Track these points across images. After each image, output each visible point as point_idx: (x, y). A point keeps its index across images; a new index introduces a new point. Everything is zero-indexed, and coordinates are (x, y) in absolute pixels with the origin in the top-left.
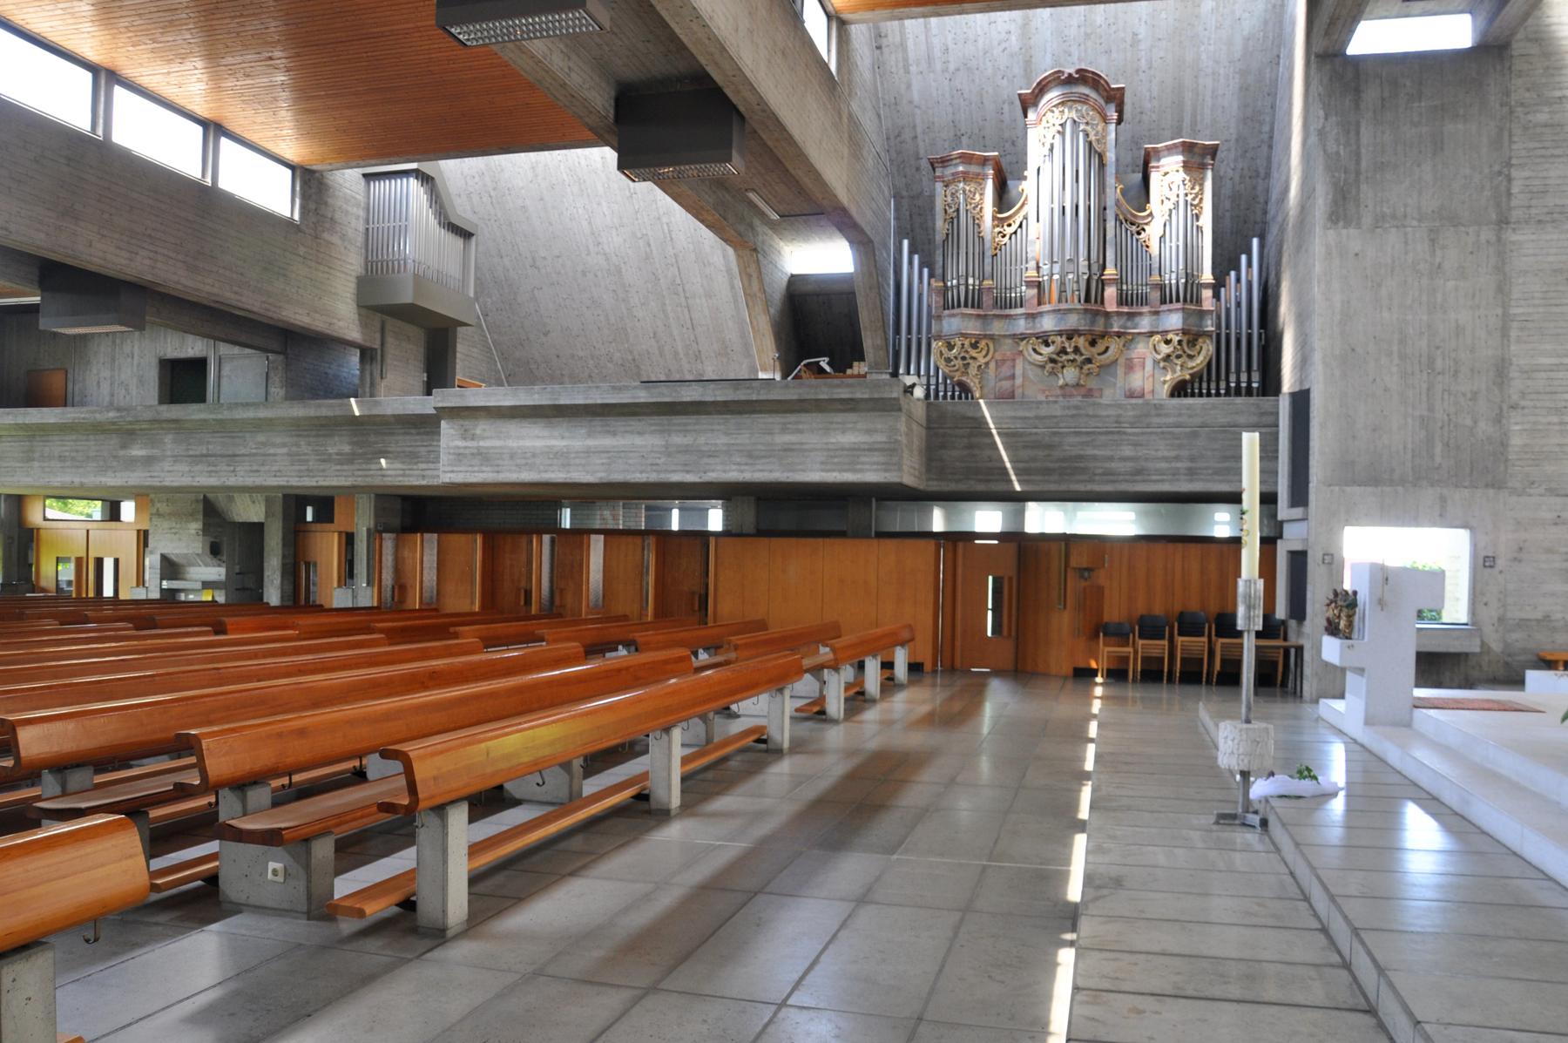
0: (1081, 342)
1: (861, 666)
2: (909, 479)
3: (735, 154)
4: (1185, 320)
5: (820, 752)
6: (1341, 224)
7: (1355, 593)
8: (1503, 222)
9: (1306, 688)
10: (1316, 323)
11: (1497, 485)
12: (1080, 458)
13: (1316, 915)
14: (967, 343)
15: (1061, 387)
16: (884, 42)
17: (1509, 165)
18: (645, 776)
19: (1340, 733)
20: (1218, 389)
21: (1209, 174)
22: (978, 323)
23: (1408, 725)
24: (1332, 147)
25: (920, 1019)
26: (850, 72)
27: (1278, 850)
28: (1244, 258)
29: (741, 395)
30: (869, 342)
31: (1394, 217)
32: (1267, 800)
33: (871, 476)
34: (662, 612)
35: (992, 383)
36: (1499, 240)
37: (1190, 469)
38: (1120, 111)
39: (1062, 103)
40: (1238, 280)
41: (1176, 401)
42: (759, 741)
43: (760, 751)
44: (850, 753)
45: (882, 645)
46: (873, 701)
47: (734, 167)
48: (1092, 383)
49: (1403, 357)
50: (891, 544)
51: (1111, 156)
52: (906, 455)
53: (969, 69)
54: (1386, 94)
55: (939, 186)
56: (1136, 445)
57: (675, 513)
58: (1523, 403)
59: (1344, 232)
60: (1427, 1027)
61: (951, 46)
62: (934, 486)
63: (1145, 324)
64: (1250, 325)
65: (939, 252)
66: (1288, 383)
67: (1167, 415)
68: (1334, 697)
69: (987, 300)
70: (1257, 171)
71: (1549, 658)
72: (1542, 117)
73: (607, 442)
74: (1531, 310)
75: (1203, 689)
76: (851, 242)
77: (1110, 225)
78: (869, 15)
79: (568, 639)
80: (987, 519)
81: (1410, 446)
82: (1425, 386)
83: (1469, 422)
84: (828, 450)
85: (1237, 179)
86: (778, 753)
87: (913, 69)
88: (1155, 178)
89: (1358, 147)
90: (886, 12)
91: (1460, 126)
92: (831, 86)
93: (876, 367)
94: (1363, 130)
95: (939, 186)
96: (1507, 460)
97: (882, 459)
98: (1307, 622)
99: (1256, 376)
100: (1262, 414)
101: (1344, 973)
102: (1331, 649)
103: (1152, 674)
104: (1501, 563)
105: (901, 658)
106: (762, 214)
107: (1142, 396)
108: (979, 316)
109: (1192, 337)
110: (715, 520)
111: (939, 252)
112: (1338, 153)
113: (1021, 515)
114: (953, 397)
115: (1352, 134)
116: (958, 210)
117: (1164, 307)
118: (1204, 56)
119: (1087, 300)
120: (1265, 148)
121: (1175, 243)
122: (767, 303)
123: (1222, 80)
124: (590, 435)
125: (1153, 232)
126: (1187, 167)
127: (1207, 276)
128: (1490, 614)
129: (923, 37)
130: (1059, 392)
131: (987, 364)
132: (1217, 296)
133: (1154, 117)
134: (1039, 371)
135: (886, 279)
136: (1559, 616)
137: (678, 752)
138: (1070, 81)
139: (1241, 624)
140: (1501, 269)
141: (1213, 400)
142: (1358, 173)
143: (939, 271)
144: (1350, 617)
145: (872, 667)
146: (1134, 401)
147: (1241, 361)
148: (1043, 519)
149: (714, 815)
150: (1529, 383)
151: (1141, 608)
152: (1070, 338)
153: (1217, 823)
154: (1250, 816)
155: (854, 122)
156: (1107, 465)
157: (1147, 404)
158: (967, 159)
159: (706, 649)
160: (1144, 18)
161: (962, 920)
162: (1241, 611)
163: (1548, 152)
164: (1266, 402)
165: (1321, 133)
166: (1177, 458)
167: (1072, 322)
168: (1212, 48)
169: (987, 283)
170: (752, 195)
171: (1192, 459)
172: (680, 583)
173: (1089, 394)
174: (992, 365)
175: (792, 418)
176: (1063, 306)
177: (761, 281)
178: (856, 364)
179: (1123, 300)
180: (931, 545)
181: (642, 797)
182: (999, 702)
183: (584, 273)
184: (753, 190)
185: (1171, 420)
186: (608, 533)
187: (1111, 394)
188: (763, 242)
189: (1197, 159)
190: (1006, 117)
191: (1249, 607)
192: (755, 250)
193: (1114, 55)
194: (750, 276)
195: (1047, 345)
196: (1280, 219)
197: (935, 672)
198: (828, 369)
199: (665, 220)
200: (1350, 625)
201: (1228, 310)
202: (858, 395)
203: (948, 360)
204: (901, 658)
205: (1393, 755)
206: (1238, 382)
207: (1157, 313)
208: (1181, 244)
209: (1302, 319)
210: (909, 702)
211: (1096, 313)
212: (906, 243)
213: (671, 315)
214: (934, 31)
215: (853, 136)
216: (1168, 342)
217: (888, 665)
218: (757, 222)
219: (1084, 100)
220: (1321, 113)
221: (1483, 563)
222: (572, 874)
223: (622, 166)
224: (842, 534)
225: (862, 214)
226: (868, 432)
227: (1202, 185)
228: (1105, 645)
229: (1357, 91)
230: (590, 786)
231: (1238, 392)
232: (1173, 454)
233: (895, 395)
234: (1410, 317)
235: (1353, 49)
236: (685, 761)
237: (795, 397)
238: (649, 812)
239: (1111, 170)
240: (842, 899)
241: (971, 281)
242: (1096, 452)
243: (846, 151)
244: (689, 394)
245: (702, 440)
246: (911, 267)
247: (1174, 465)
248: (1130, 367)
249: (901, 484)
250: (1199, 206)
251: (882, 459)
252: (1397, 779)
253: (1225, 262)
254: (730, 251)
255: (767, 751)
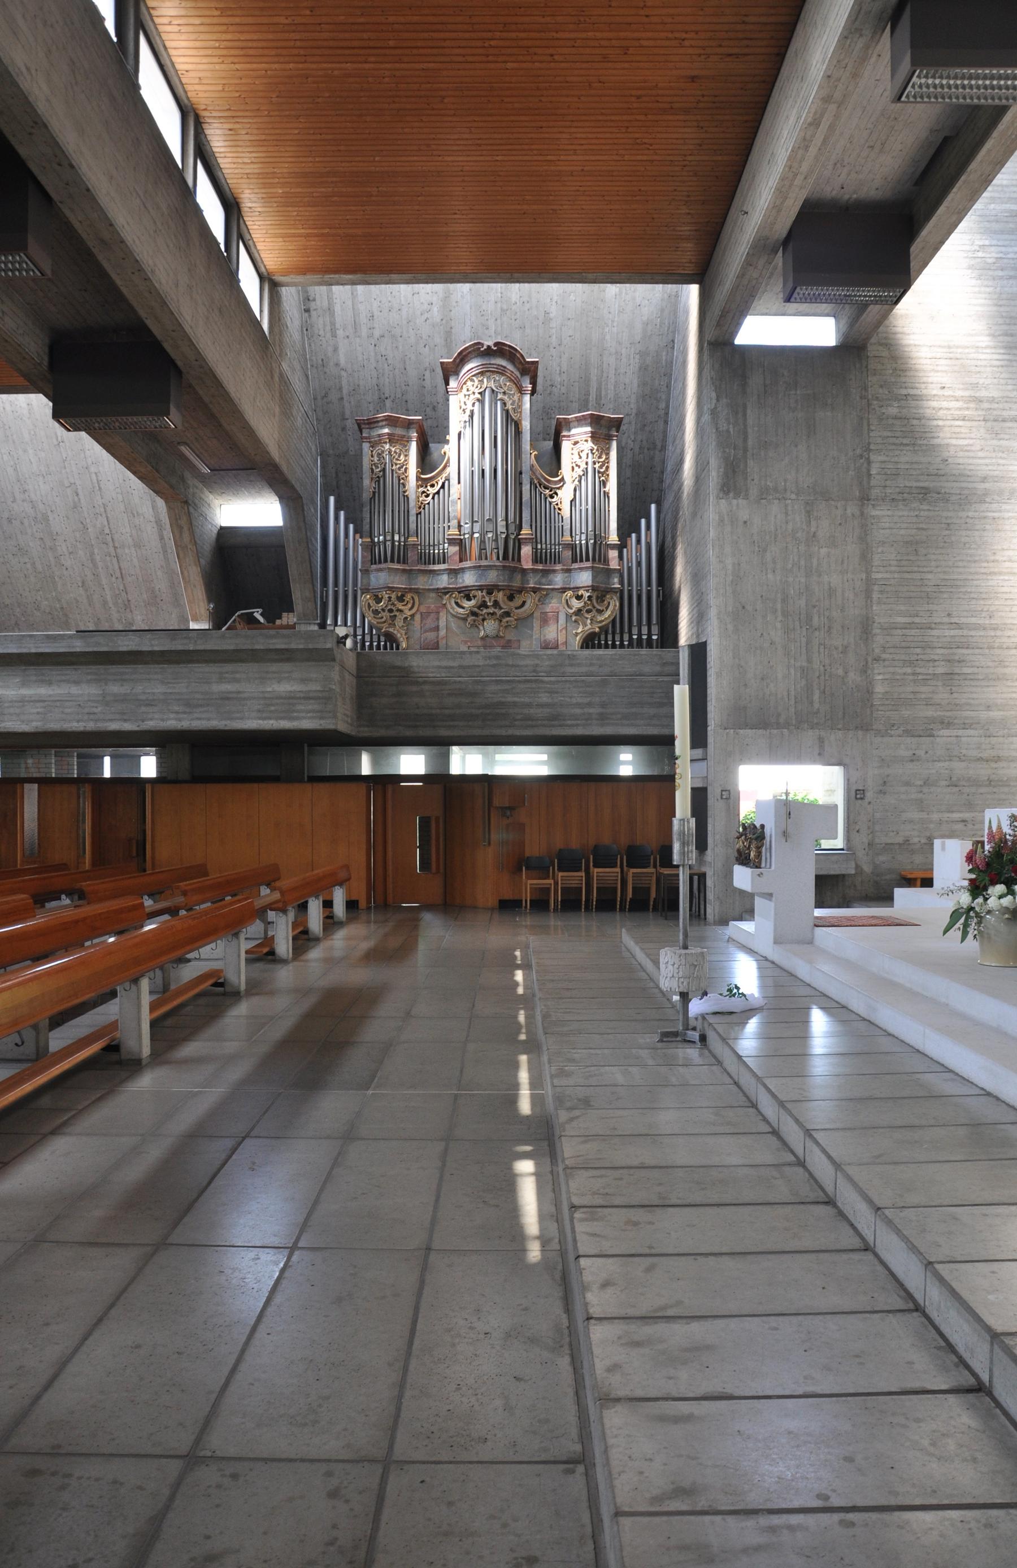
0: (500, 596)
1: (303, 907)
2: (343, 727)
3: (173, 409)
4: (594, 578)
5: (272, 993)
6: (731, 495)
7: (763, 826)
8: (865, 498)
9: (709, 910)
10: (712, 583)
11: (865, 727)
12: (502, 704)
13: (765, 1120)
14: (393, 596)
15: (482, 638)
16: (312, 305)
17: (868, 450)
18: (114, 1026)
19: (750, 951)
20: (622, 641)
21: (614, 444)
22: (404, 578)
23: (811, 942)
24: (723, 426)
25: (429, 1249)
26: (281, 334)
27: (719, 1063)
28: (643, 521)
29: (178, 645)
30: (298, 594)
31: (776, 490)
32: (703, 1017)
33: (307, 724)
34: (100, 859)
35: (417, 635)
36: (862, 514)
37: (601, 714)
38: (534, 383)
39: (482, 373)
40: (639, 541)
41: (587, 652)
42: (216, 984)
43: (218, 994)
44: (301, 992)
45: (322, 886)
46: (317, 939)
47: (173, 421)
48: (511, 635)
49: (786, 614)
50: (323, 788)
51: (526, 425)
52: (339, 704)
53: (393, 336)
54: (768, 382)
55: (366, 446)
56: (551, 692)
57: (107, 760)
58: (884, 656)
59: (735, 502)
60: (887, 1212)
61: (376, 313)
62: (366, 732)
63: (558, 580)
64: (649, 583)
65: (366, 509)
66: (685, 635)
67: (579, 665)
68: (741, 919)
69: (412, 556)
70: (654, 443)
71: (909, 876)
72: (893, 411)
73: (43, 691)
74: (888, 576)
75: (618, 916)
76: (281, 499)
77: (526, 488)
78: (299, 279)
79: (13, 892)
80: (412, 763)
81: (793, 693)
82: (804, 640)
83: (840, 672)
84: (263, 700)
85: (637, 450)
86: (235, 995)
87: (340, 333)
88: (566, 446)
89: (745, 426)
90: (316, 277)
91: (829, 414)
92: (265, 346)
93: (305, 618)
94: (749, 411)
95: (366, 446)
96: (872, 705)
97: (316, 707)
98: (709, 852)
99: (655, 629)
100: (664, 664)
101: (801, 1170)
102: (742, 877)
103: (571, 903)
104: (869, 795)
105: (339, 897)
106: (193, 468)
107: (557, 647)
108: (404, 570)
109: (600, 593)
110: (148, 767)
111: (366, 509)
112: (728, 431)
113: (446, 759)
114: (378, 647)
115: (740, 415)
116: (384, 470)
117: (576, 566)
118: (608, 337)
119: (505, 557)
120: (661, 423)
121: (586, 504)
122: (198, 555)
123: (624, 360)
124: (24, 684)
125: (565, 495)
126: (594, 437)
127: (613, 538)
128: (861, 840)
129: (349, 303)
130: (480, 643)
131: (413, 616)
132: (621, 557)
133: (564, 390)
134: (461, 623)
135: (314, 533)
136: (916, 840)
137: (146, 999)
138: (489, 352)
139: (676, 859)
140: (864, 539)
141: (618, 651)
142: (745, 450)
143: (366, 527)
144: (759, 848)
145: (315, 907)
146: (549, 652)
147: (643, 615)
148: (466, 762)
149: (186, 1061)
150: (888, 638)
151: (559, 843)
152: (490, 593)
153: (661, 1041)
154: (690, 1033)
155: (284, 382)
156: (526, 711)
157: (561, 654)
158: (392, 422)
159: (151, 895)
160: (555, 298)
161: (446, 1150)
162: (676, 847)
163: (897, 441)
164: (667, 653)
165: (713, 412)
166: (589, 705)
167: (492, 577)
168: (615, 330)
169: (412, 539)
170: (184, 449)
171: (603, 705)
172: (117, 829)
173: (508, 645)
174: (418, 617)
175: (229, 667)
176: (484, 563)
177: (192, 533)
178: (285, 614)
179: (537, 558)
180: (363, 787)
181: (113, 1048)
182: (435, 932)
183: (10, 520)
184: (185, 444)
185: (584, 669)
186: (44, 782)
187: (528, 646)
188: (194, 494)
189: (604, 431)
190: (428, 383)
191: (683, 844)
192: (186, 502)
193: (528, 331)
194: (181, 528)
195: (469, 599)
196: (675, 487)
197: (369, 908)
198: (261, 620)
199: (93, 469)
200: (759, 855)
201: (630, 569)
202: (293, 646)
203: (376, 612)
204: (339, 897)
205: (802, 969)
206: (640, 634)
207: (569, 571)
208: (590, 507)
209: (697, 578)
210: (348, 938)
211: (514, 570)
212: (332, 499)
213: (100, 564)
214: (361, 298)
215: (282, 391)
216: (579, 598)
217: (328, 904)
218: (187, 475)
219: (501, 371)
220: (714, 395)
221: (855, 795)
222: (55, 1132)
223: (56, 416)
224: (276, 779)
225: (294, 472)
226: (303, 681)
227: (608, 454)
228: (528, 878)
229: (744, 377)
230: (57, 1040)
231: (640, 644)
232: (587, 700)
233: (329, 646)
234: (791, 579)
235: (740, 340)
236: (153, 1007)
237: (232, 647)
238: (120, 1063)
239: (526, 437)
240: (328, 1137)
241: (396, 538)
242: (516, 699)
243: (277, 410)
244: (126, 644)
245: (139, 689)
246: (337, 523)
247: (586, 710)
248: (545, 621)
249: (335, 731)
250: (606, 473)
251: (316, 707)
252: (807, 991)
253: (628, 526)
254: (160, 503)
255: (224, 994)
